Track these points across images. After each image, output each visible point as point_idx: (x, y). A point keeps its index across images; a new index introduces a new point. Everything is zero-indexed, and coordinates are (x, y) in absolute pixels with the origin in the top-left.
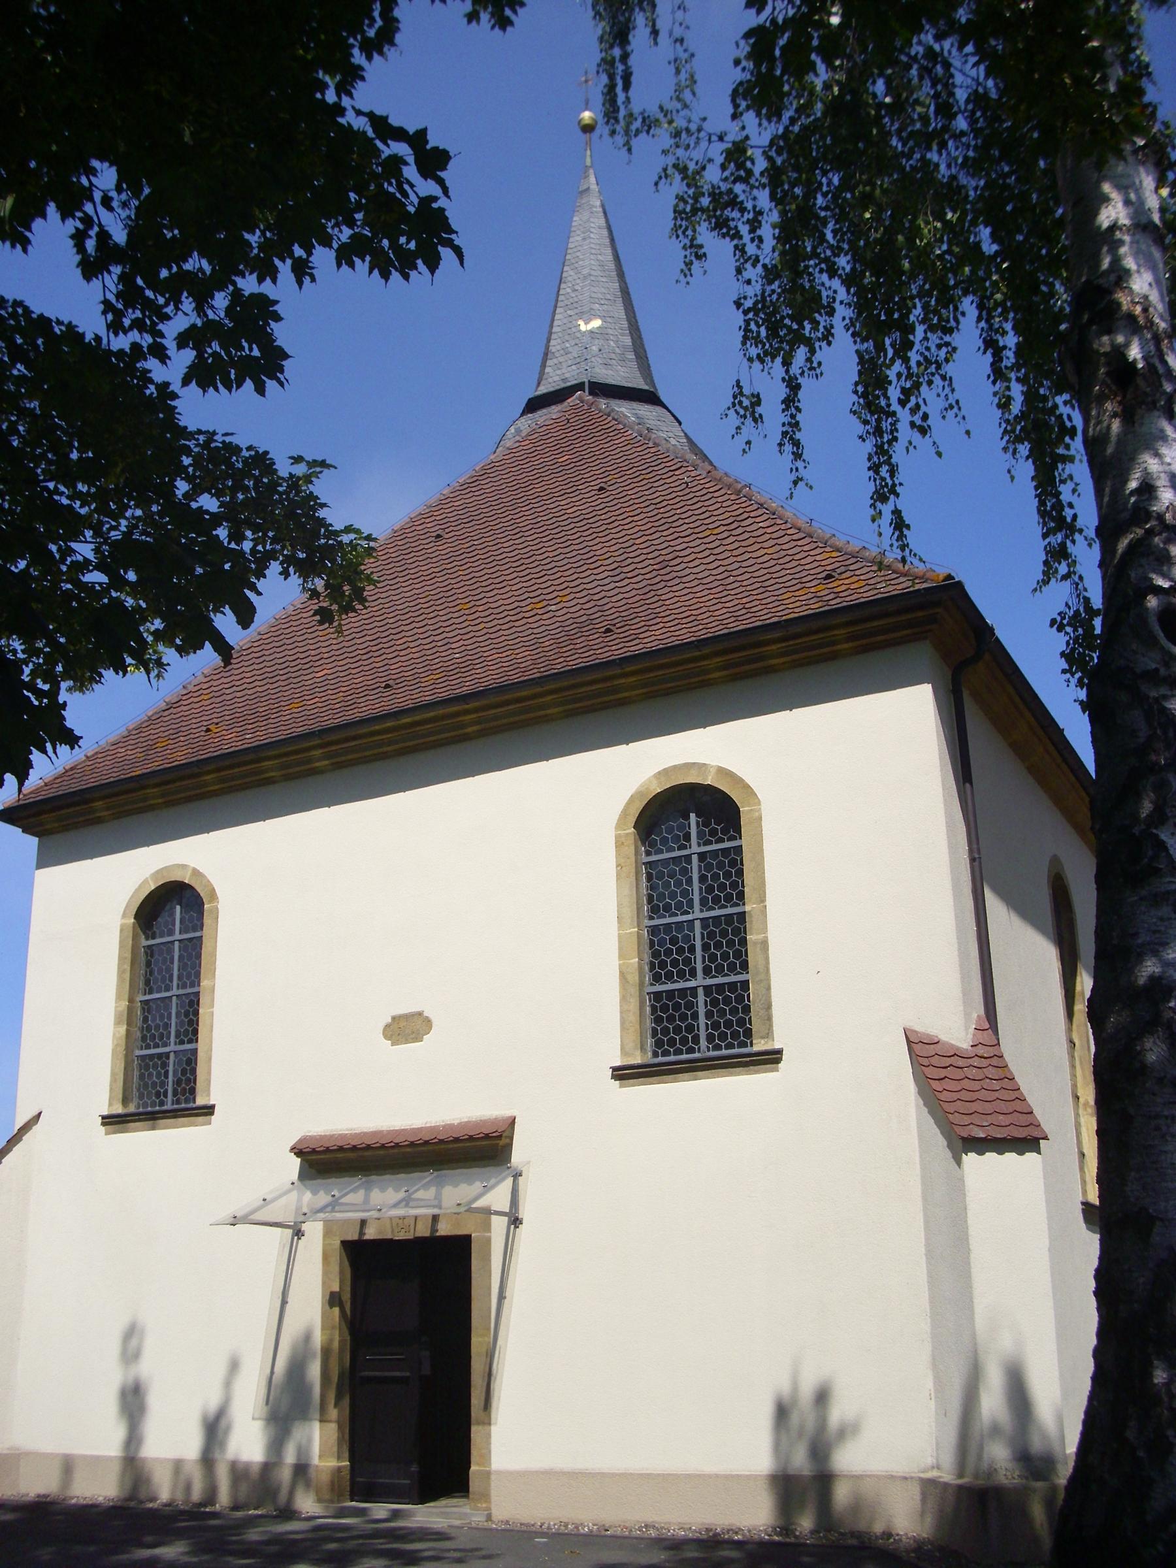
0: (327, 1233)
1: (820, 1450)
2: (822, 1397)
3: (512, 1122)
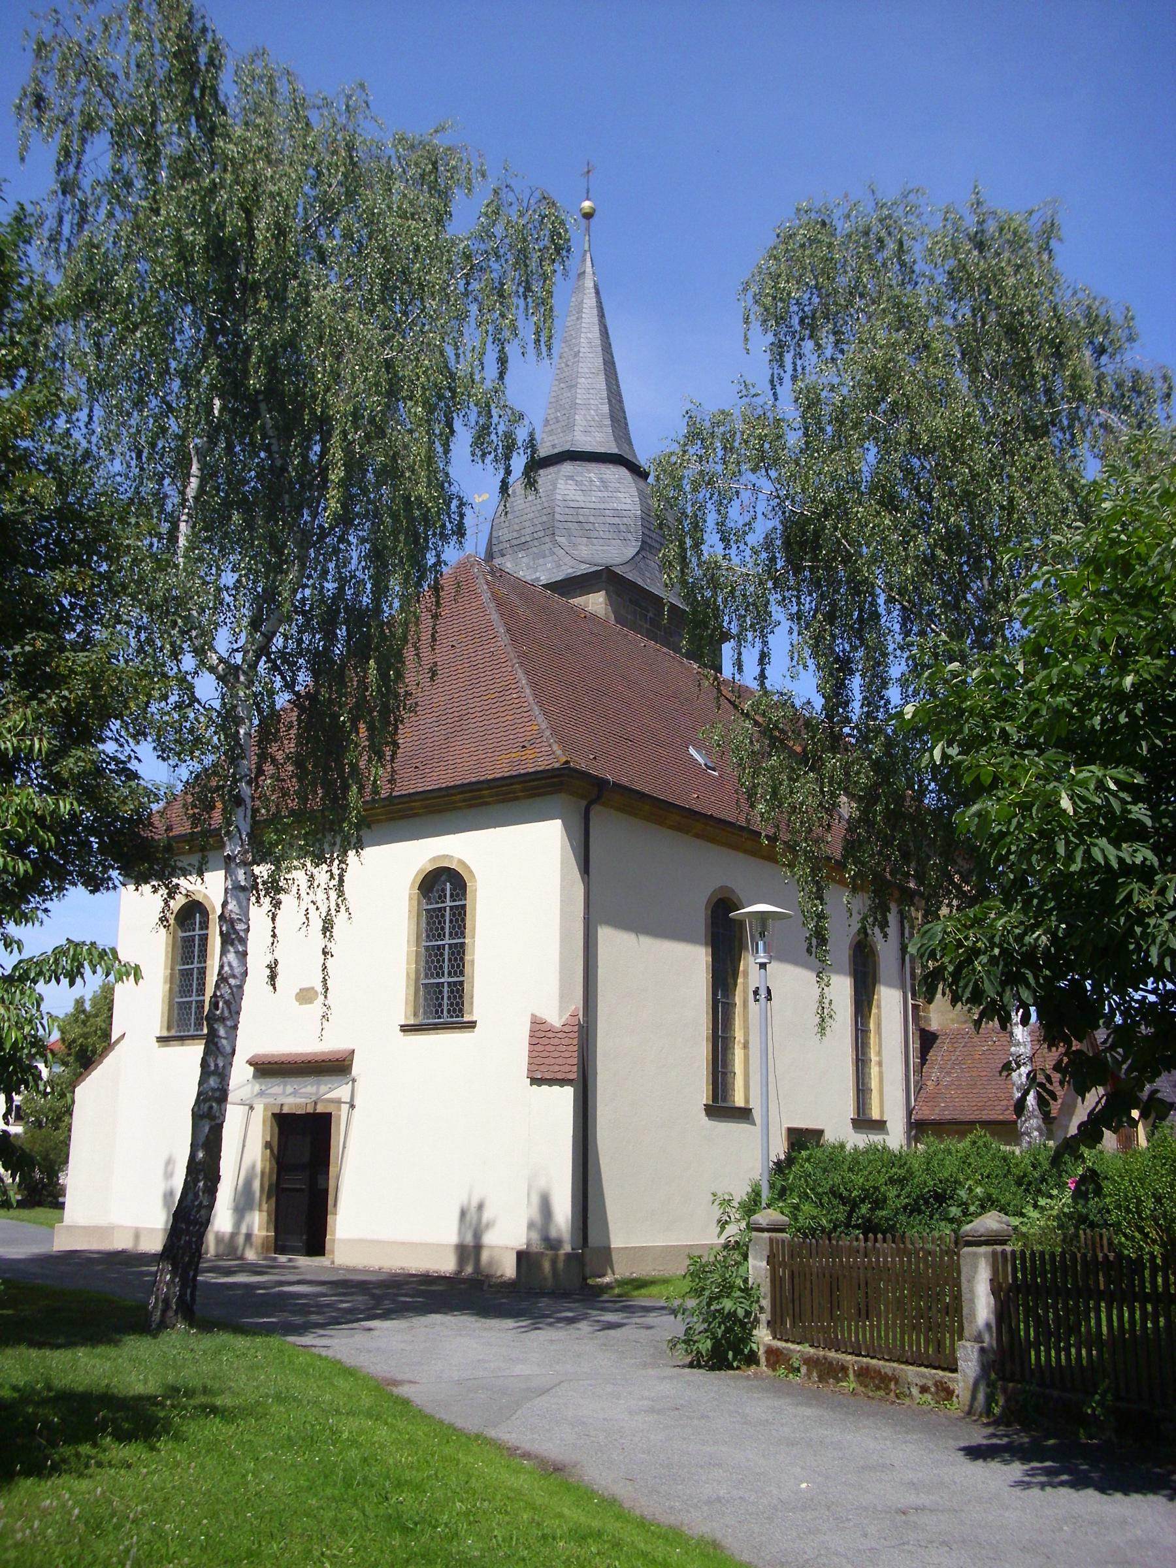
0: (265, 1109)
1: (477, 1235)
2: (480, 1207)
3: (353, 1051)
